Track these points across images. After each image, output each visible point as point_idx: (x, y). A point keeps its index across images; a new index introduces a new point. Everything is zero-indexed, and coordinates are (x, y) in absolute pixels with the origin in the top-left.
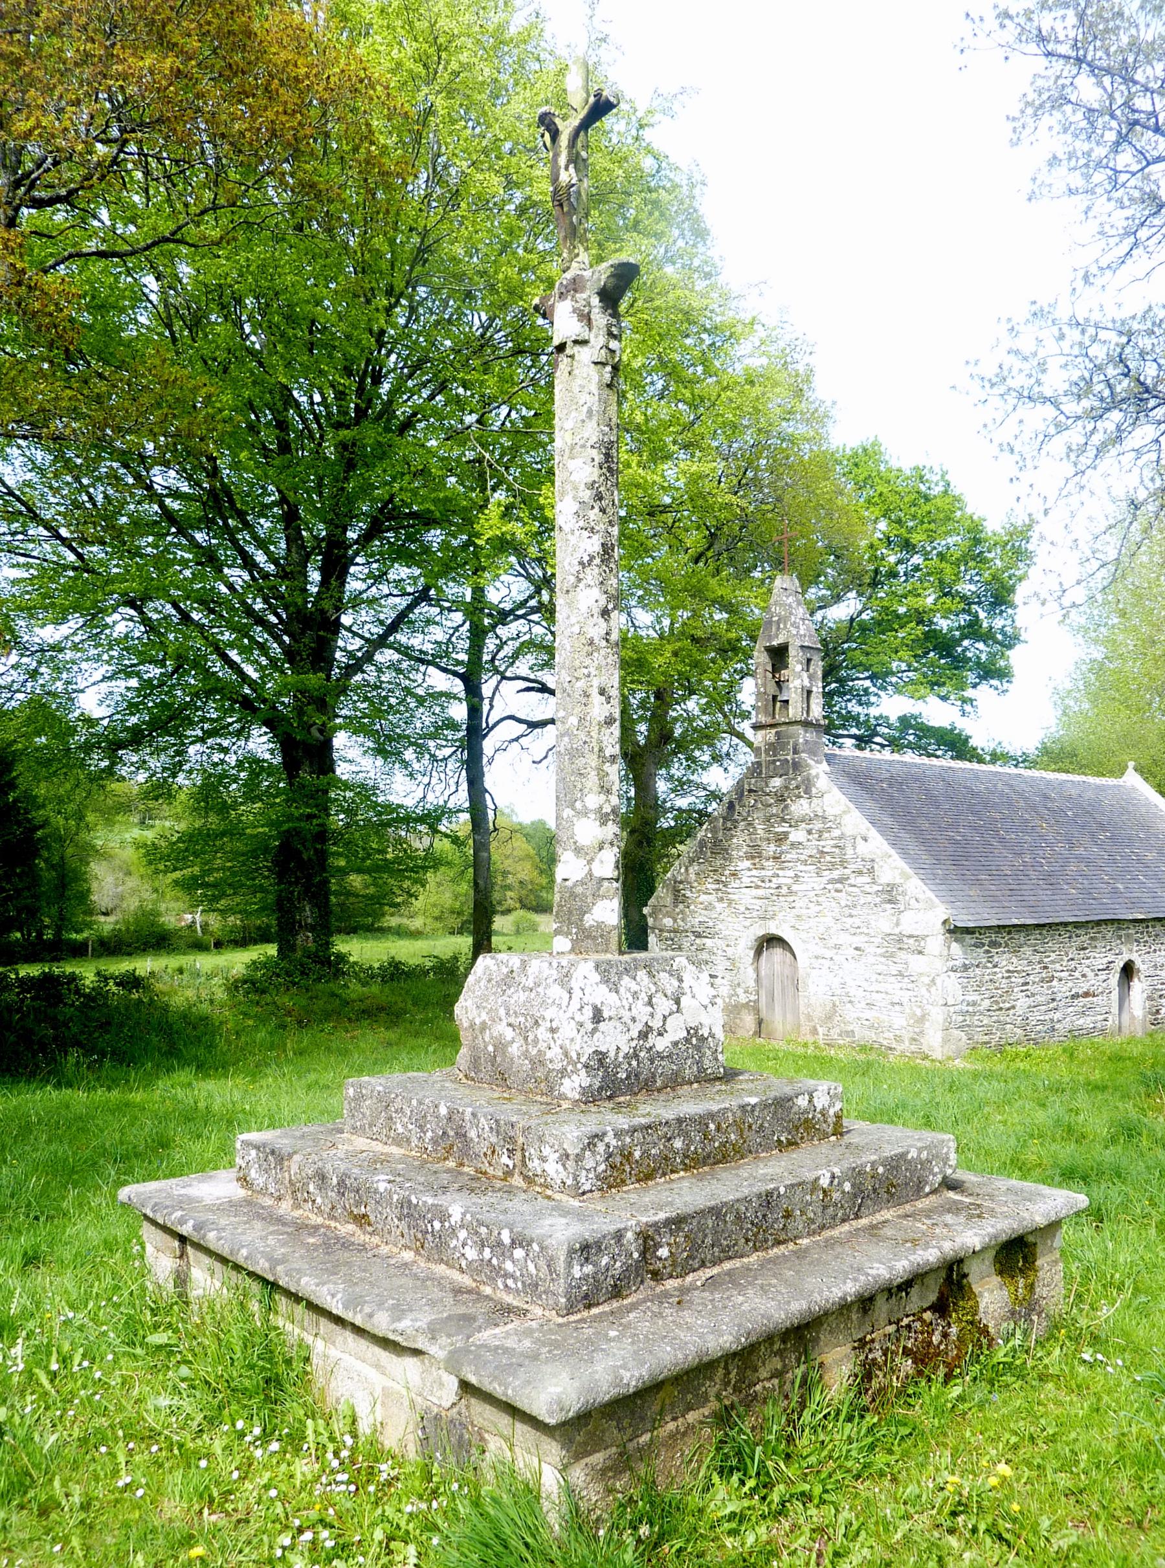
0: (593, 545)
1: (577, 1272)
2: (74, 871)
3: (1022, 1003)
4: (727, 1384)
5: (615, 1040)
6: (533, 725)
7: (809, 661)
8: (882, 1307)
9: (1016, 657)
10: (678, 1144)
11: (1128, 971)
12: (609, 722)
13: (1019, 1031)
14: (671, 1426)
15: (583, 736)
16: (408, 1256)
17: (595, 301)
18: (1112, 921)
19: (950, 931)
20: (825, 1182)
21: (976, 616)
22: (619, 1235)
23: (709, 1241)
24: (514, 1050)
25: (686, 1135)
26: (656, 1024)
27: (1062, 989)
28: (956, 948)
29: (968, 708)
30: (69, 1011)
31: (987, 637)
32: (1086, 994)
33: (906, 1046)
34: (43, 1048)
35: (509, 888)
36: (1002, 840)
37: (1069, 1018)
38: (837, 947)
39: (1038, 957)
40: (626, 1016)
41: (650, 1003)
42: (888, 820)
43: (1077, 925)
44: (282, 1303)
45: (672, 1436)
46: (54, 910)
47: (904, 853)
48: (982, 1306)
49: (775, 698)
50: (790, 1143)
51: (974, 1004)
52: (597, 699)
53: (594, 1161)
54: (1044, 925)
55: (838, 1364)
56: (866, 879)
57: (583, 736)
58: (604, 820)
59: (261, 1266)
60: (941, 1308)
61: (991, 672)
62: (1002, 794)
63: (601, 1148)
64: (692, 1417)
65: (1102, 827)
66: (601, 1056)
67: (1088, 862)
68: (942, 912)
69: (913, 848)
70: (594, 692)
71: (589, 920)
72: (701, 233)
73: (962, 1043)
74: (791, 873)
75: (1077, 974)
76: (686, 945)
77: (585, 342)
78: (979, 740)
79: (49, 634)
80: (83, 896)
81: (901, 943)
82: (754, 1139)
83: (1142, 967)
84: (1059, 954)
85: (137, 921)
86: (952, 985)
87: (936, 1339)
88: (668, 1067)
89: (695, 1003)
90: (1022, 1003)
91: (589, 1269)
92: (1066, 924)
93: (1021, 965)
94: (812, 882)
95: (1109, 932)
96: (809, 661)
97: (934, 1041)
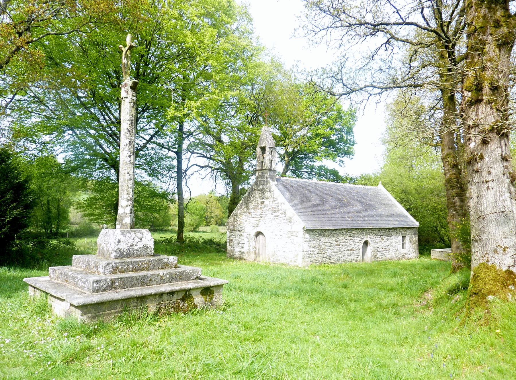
0: (128, 141)
1: (95, 285)
2: (63, 209)
3: (329, 252)
4: (122, 306)
5: (123, 246)
6: (202, 167)
7: (272, 151)
8: (165, 296)
9: (355, 148)
10: (131, 266)
11: (366, 243)
12: (130, 179)
13: (328, 260)
14: (108, 312)
15: (124, 183)
16: (73, 287)
17: (129, 89)
18: (361, 229)
19: (305, 231)
20: (161, 274)
21: (343, 136)
22: (106, 280)
23: (129, 283)
24: (105, 249)
25: (133, 265)
26: (135, 243)
27: (343, 248)
28: (307, 235)
29: (341, 164)
30: (46, 251)
31: (345, 142)
32: (351, 250)
33: (292, 264)
34: (38, 261)
35: (212, 217)
36: (330, 205)
37: (345, 256)
38: (276, 235)
39: (335, 239)
40: (127, 242)
41: (134, 239)
42: (293, 198)
43: (348, 230)
44: (48, 296)
45: (107, 313)
46: (56, 223)
47: (296, 208)
48: (195, 301)
49: (262, 162)
50: (162, 268)
51: (313, 251)
52: (127, 175)
53: (109, 268)
54: (337, 229)
55: (152, 308)
56: (284, 215)
57: (124, 183)
58: (128, 200)
59: (43, 289)
60: (183, 299)
61: (348, 153)
62: (334, 191)
63: (111, 265)
64: (112, 311)
65: (366, 201)
66: (120, 250)
67: (357, 211)
68: (303, 225)
69: (299, 206)
70: (126, 173)
71: (124, 222)
72: (250, 20)
73: (309, 263)
74: (265, 214)
75: (348, 244)
76: (237, 234)
77: (127, 98)
78: (342, 173)
79: (47, 138)
80: (66, 218)
81: (292, 233)
82: (151, 267)
83: (371, 242)
84: (342, 239)
85: (84, 226)
86: (306, 246)
87: (181, 306)
88: (138, 253)
89: (146, 240)
90: (329, 252)
91: (98, 285)
92: (345, 229)
93: (329, 241)
94: (270, 216)
95: (360, 232)
96: (272, 151)
97: (300, 263)
